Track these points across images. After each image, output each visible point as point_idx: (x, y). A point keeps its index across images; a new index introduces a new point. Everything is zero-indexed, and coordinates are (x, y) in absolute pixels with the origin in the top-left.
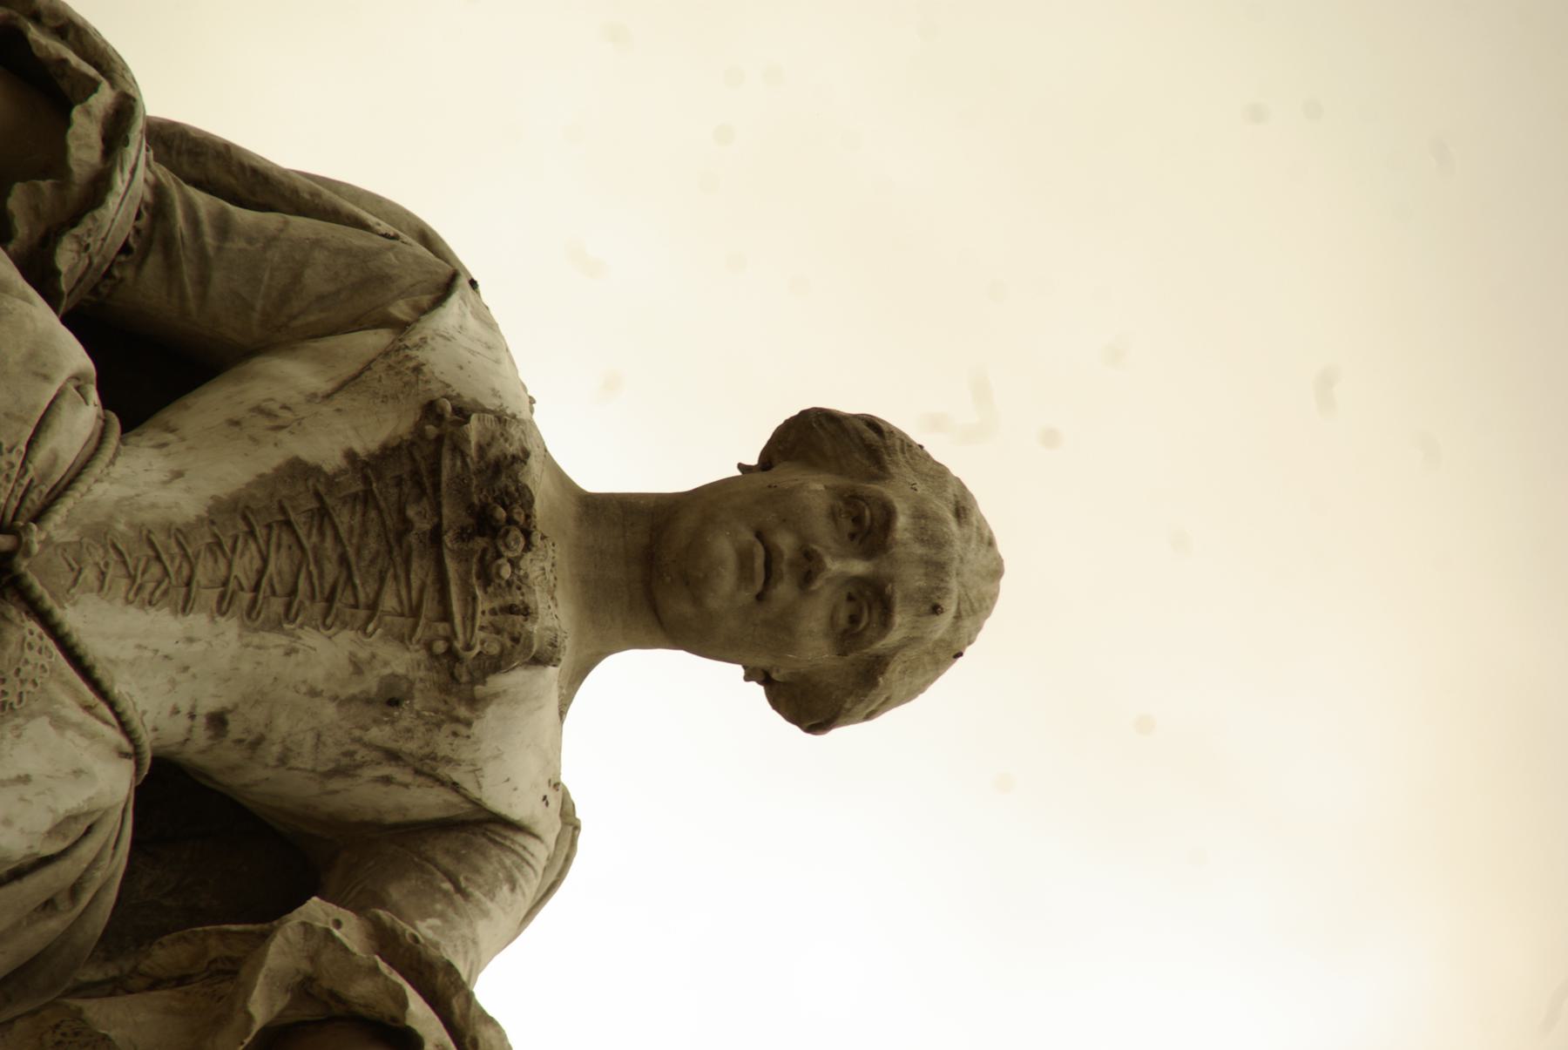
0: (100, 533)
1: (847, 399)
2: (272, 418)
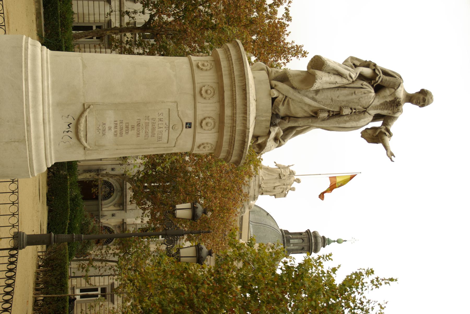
0: (372, 107)
1: (426, 88)
2: (385, 97)
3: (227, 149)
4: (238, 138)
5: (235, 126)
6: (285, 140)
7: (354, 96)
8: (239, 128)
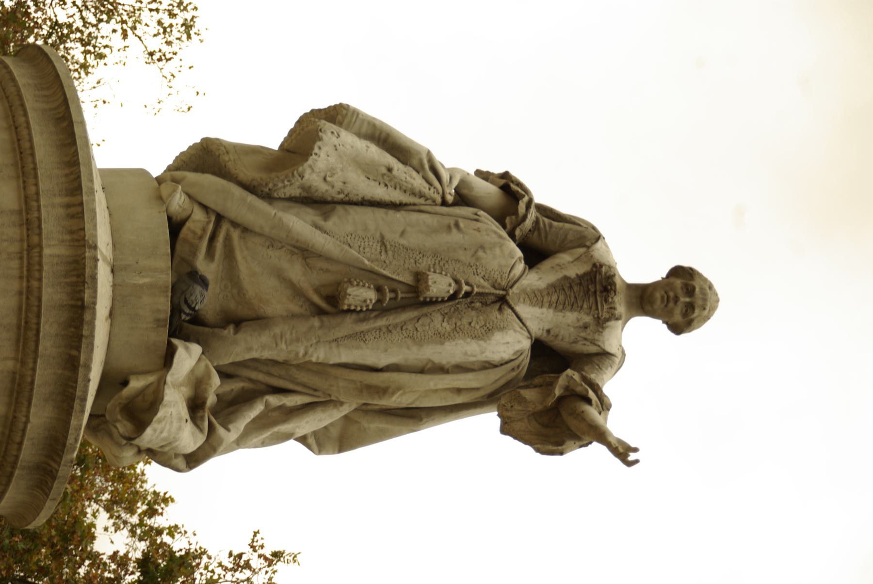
0: (524, 291)
1: (686, 262)
2: (561, 267)
3: (10, 364)
4: (51, 294)
5: (40, 246)
6: (231, 426)
7: (455, 237)
8: (53, 249)
